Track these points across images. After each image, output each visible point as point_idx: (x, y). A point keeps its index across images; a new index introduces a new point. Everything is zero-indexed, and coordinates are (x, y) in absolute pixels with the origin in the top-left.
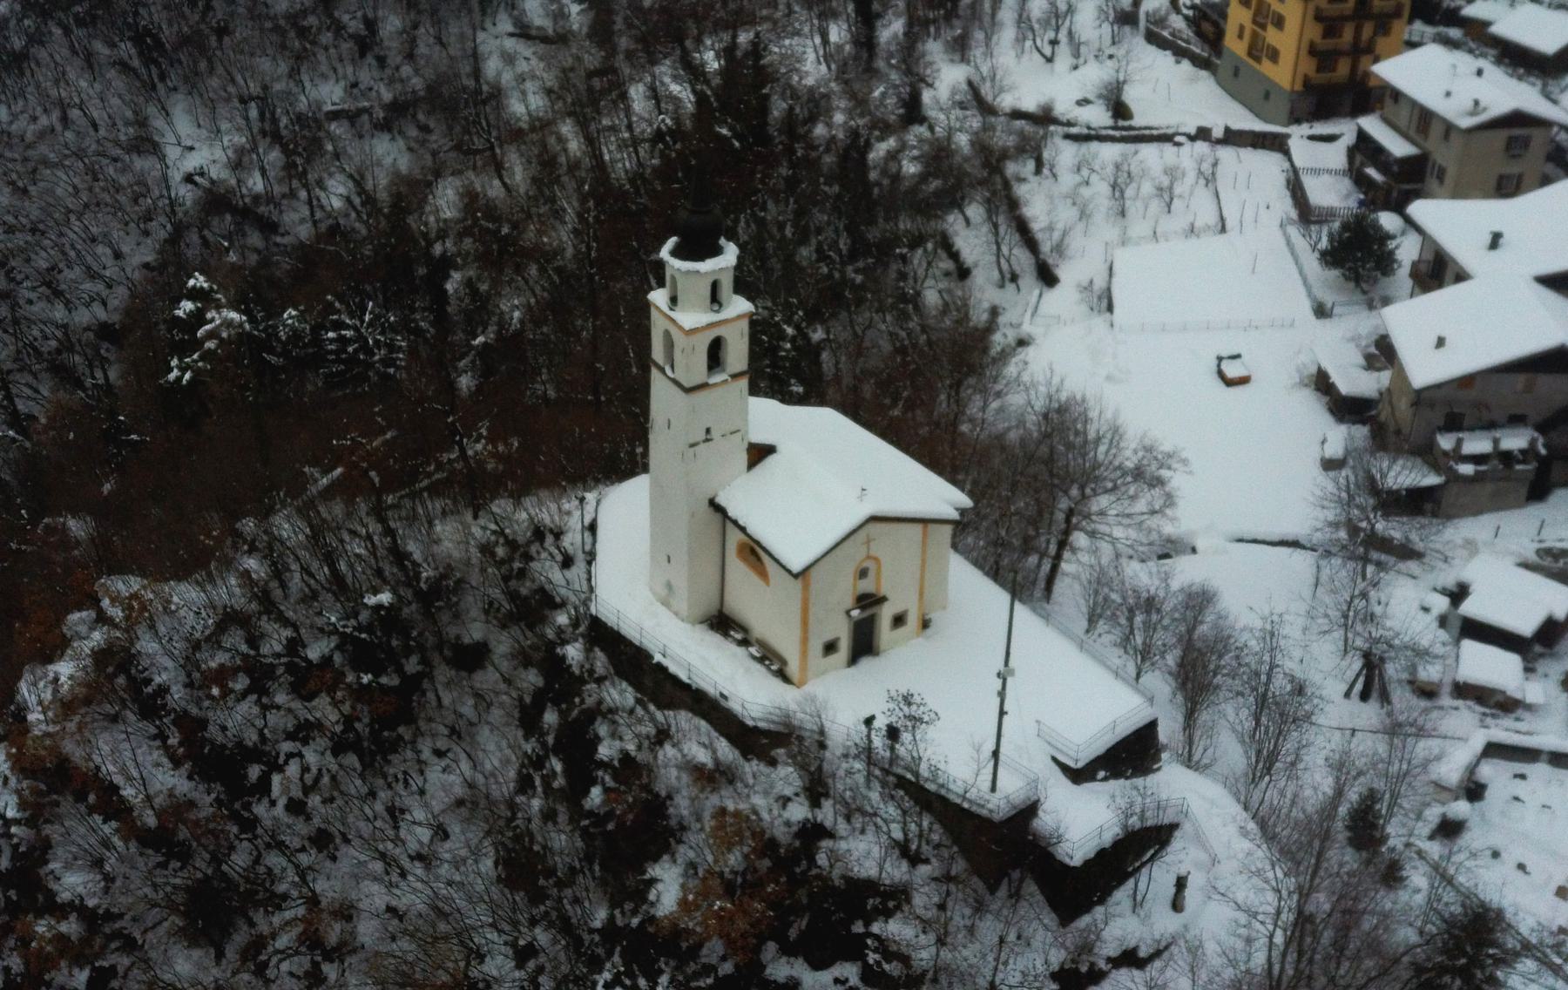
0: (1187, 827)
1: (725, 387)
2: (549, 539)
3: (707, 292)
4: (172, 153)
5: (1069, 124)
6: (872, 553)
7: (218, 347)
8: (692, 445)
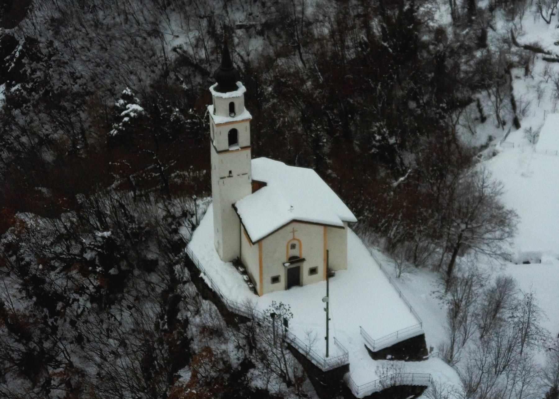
0: (430, 389)
1: (239, 152)
2: (189, 216)
3: (227, 107)
4: (168, 37)
5: (548, 53)
6: (296, 237)
7: (129, 120)
8: (222, 178)
